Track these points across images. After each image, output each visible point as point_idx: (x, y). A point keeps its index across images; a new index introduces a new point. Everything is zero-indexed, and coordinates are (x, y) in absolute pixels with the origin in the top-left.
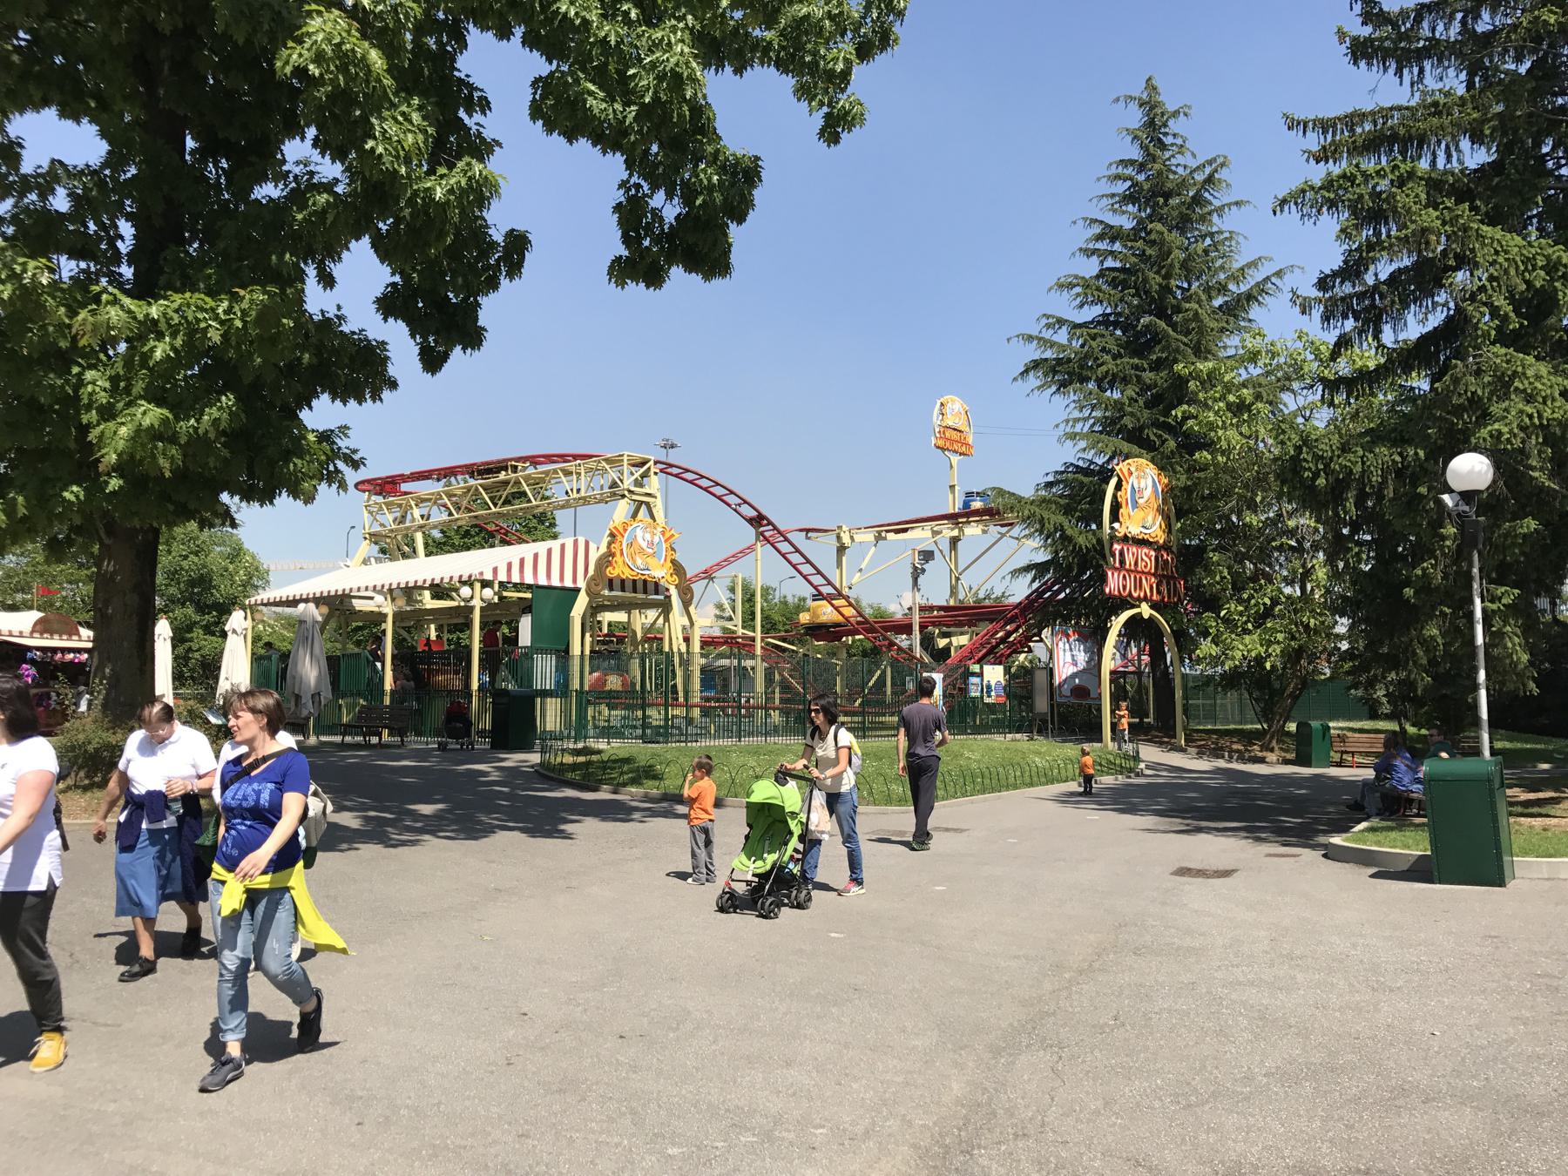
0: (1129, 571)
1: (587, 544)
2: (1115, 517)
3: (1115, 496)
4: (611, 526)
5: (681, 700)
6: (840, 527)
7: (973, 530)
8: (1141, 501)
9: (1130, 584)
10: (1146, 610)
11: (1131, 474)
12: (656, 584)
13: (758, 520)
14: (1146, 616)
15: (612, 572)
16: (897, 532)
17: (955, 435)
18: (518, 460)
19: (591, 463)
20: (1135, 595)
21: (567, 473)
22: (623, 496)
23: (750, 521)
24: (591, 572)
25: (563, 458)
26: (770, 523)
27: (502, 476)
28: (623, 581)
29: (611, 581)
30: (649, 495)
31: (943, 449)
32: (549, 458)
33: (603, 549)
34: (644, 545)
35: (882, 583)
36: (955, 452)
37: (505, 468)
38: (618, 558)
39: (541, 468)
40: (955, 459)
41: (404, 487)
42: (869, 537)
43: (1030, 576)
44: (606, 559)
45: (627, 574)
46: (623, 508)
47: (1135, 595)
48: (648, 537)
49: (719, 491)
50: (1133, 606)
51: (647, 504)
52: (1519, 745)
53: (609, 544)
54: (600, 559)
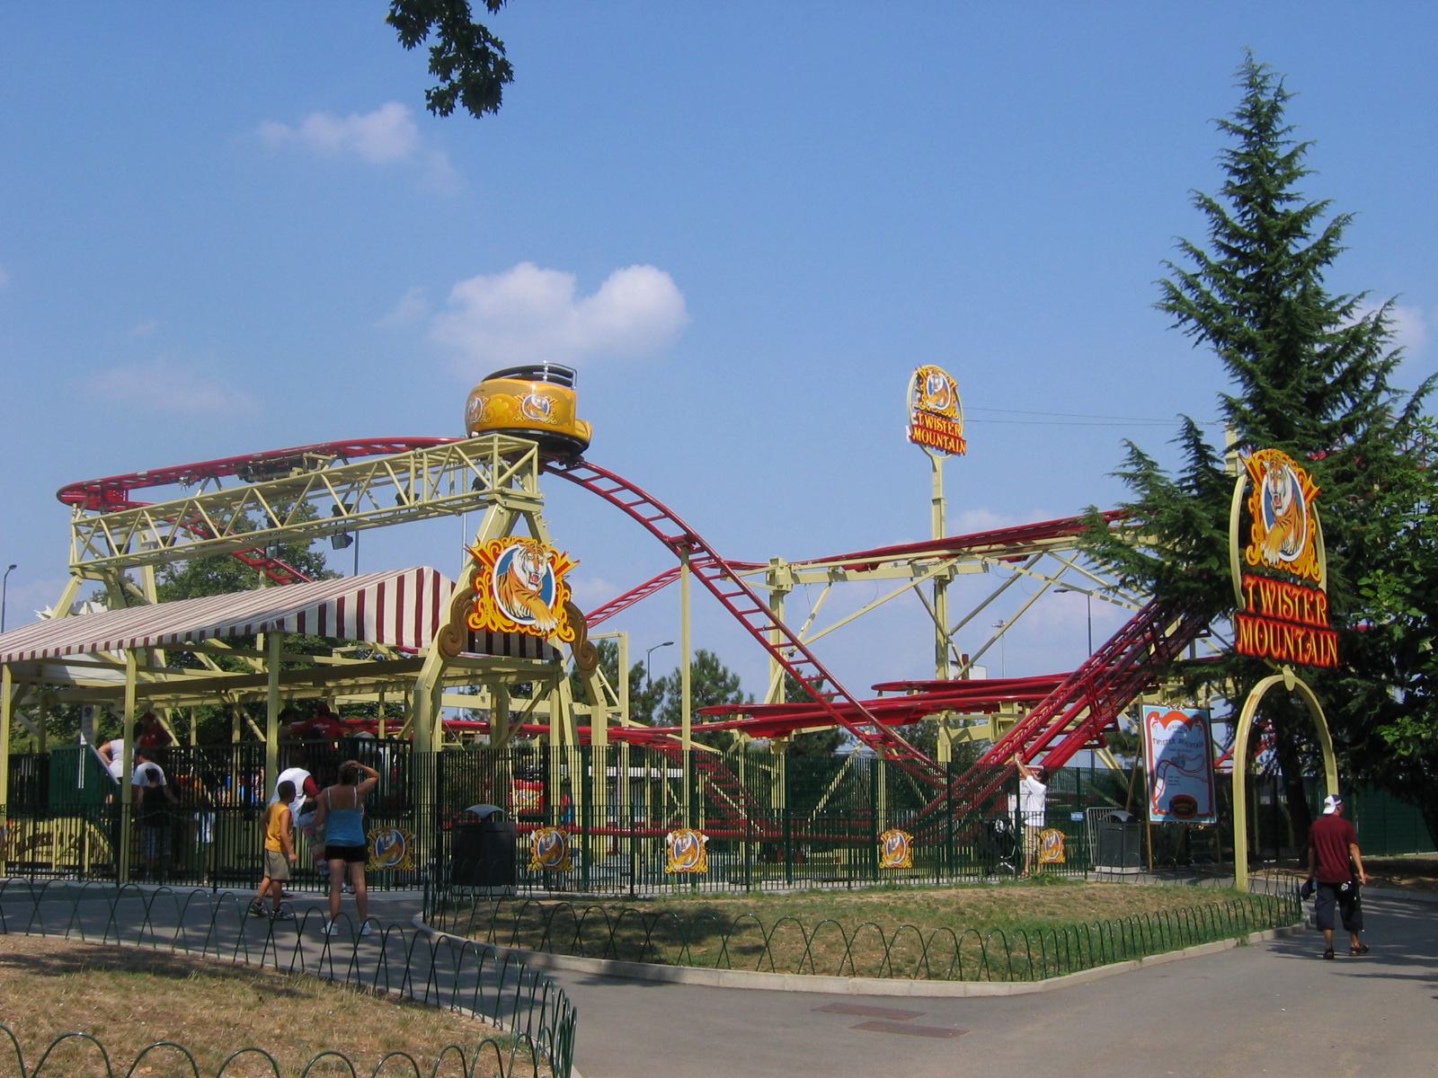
0: (1266, 618)
1: (437, 577)
2: (1245, 540)
3: (1244, 508)
4: (919, 370)
5: (578, 822)
6: (775, 561)
7: (969, 567)
8: (1279, 513)
9: (1269, 638)
10: (1289, 677)
11: (1264, 472)
12: (540, 642)
13: (686, 544)
14: (1290, 687)
15: (477, 621)
16: (863, 568)
17: (940, 425)
18: (316, 450)
19: (437, 453)
20: (1276, 654)
21: (399, 467)
22: (494, 502)
23: (672, 544)
24: (445, 619)
25: (389, 445)
26: (703, 548)
27: (295, 474)
28: (489, 634)
29: (472, 633)
30: (530, 500)
31: (921, 443)
32: (368, 447)
33: (463, 585)
34: (524, 578)
35: (869, 642)
36: (940, 448)
37: (299, 463)
38: (486, 599)
39: (355, 462)
40: (940, 459)
41: (134, 495)
42: (821, 573)
43: (674, 680)
44: (466, 604)
45: (499, 625)
46: (492, 518)
47: (1276, 654)
48: (530, 566)
49: (626, 497)
50: (1271, 672)
51: (528, 515)
52: (1399, 857)
53: (473, 577)
54: (459, 600)
